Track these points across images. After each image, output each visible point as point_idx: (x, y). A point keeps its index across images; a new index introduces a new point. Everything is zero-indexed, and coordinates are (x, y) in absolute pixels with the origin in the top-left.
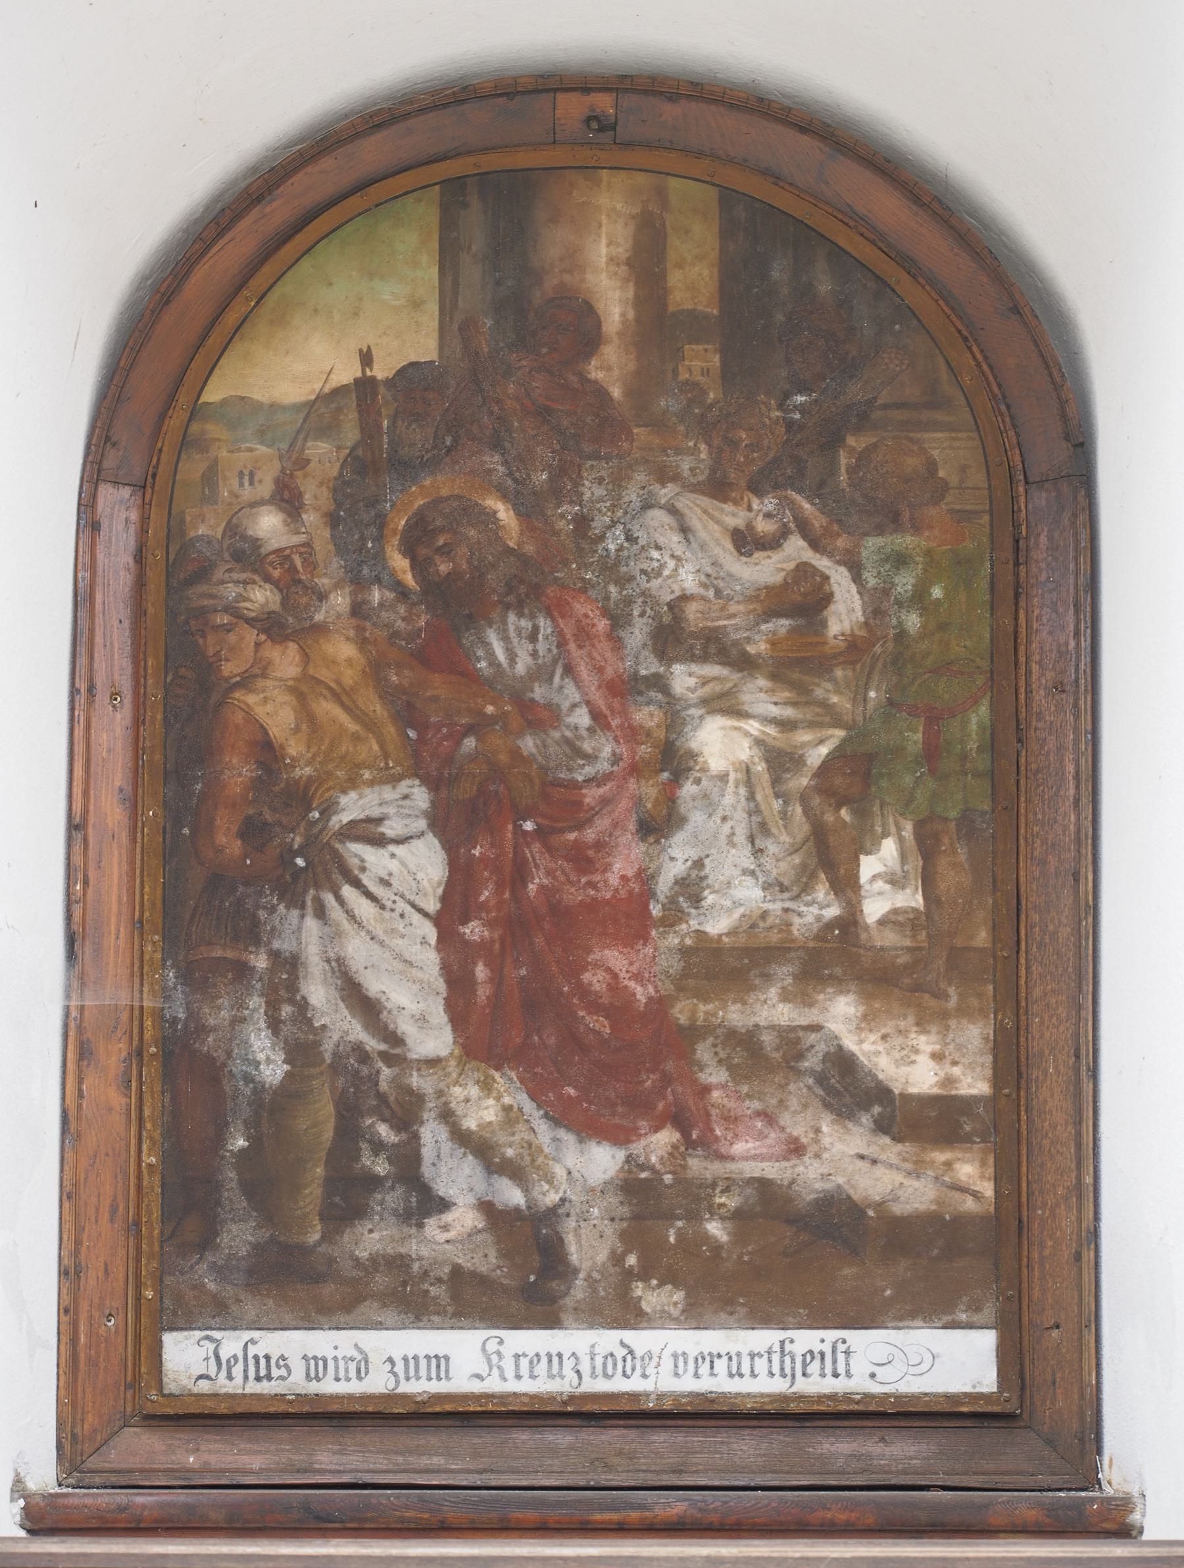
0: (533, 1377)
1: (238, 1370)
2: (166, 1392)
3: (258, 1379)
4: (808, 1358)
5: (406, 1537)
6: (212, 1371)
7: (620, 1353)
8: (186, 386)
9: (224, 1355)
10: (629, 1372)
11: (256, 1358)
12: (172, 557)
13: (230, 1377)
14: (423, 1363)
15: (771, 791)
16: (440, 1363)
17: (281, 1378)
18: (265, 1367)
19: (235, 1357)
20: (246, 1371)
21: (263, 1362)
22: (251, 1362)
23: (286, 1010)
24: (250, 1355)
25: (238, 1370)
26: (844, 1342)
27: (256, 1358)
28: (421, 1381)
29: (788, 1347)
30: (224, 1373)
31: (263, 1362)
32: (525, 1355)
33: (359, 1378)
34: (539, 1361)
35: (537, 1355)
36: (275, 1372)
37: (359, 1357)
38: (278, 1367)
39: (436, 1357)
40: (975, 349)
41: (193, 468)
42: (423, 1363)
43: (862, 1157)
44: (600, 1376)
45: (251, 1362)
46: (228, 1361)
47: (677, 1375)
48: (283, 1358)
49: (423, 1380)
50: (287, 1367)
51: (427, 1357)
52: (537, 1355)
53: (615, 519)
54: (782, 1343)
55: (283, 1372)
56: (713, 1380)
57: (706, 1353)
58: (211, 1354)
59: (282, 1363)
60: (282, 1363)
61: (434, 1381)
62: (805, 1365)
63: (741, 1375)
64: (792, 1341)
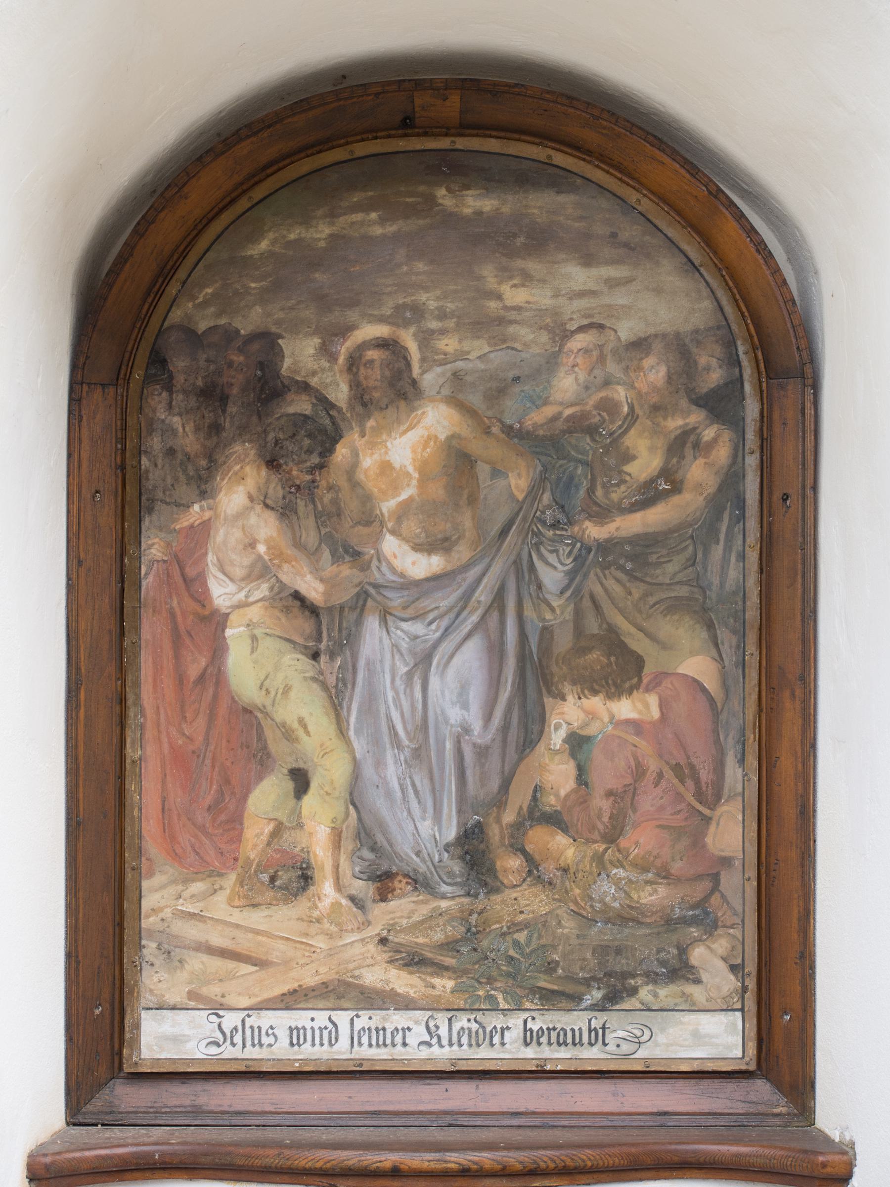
1: (238, 1039)
2: (752, 1067)
9: (227, 1027)
11: (252, 1027)
12: (487, 560)
14: (569, 1040)
17: (270, 1045)
21: (256, 1031)
22: (248, 1032)
24: (247, 1025)
25: (238, 1039)
28: (363, 1048)
30: (229, 1041)
32: (554, 1029)
33: (331, 1044)
34: (464, 1033)
36: (265, 1040)
37: (330, 1026)
38: (267, 1034)
42: (569, 1040)
43: (267, 677)
44: (555, 1044)
45: (248, 1032)
48: (272, 1028)
49: (455, 1047)
53: (576, 369)
54: (525, 1022)
55: (271, 1040)
59: (270, 1032)
60: (270, 1032)
63: (385, 1045)
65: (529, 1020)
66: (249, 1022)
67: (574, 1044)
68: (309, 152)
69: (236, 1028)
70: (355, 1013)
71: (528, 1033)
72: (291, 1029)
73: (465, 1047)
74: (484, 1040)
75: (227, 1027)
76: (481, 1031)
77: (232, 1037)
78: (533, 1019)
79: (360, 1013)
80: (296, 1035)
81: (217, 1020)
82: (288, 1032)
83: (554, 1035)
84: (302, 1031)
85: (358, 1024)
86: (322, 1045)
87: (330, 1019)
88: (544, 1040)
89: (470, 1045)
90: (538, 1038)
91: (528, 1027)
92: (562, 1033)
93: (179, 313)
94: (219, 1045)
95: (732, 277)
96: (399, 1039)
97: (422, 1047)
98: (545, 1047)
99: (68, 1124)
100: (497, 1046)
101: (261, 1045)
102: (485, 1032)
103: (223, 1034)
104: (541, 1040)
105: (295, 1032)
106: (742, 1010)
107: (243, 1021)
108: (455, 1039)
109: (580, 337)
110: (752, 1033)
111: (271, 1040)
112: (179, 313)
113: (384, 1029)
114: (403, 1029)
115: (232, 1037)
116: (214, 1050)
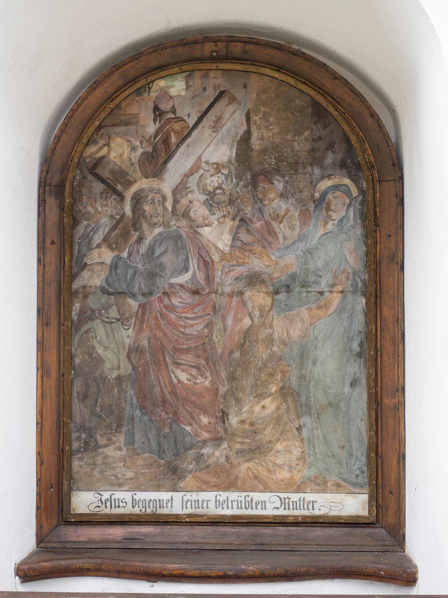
1: (108, 504)
2: (373, 519)
3: (293, 509)
5: (274, 581)
6: (100, 505)
8: (325, 83)
10: (247, 507)
11: (115, 499)
13: (106, 507)
16: (263, 504)
18: (250, 504)
19: (107, 499)
20: (191, 505)
21: (117, 501)
25: (108, 504)
26: (248, 496)
27: (115, 499)
29: (218, 498)
30: (104, 505)
31: (117, 501)
32: (234, 501)
34: (310, 503)
36: (121, 504)
41: (80, 230)
46: (138, 501)
47: (216, 508)
52: (224, 500)
54: (216, 496)
59: (123, 501)
62: (149, 503)
63: (297, 509)
64: (220, 496)
65: (218, 496)
66: (113, 497)
69: (168, 500)
71: (218, 502)
74: (219, 506)
77: (222, 505)
78: (220, 496)
80: (184, 504)
81: (100, 497)
85: (185, 499)
86: (232, 508)
90: (222, 505)
91: (218, 499)
92: (144, 501)
93: (78, 178)
95: (272, 65)
96: (205, 505)
97: (275, 510)
98: (299, 510)
99: (37, 548)
101: (119, 507)
103: (102, 503)
107: (216, 496)
112: (78, 178)
113: (198, 501)
114: (207, 500)
115: (106, 503)
116: (97, 509)
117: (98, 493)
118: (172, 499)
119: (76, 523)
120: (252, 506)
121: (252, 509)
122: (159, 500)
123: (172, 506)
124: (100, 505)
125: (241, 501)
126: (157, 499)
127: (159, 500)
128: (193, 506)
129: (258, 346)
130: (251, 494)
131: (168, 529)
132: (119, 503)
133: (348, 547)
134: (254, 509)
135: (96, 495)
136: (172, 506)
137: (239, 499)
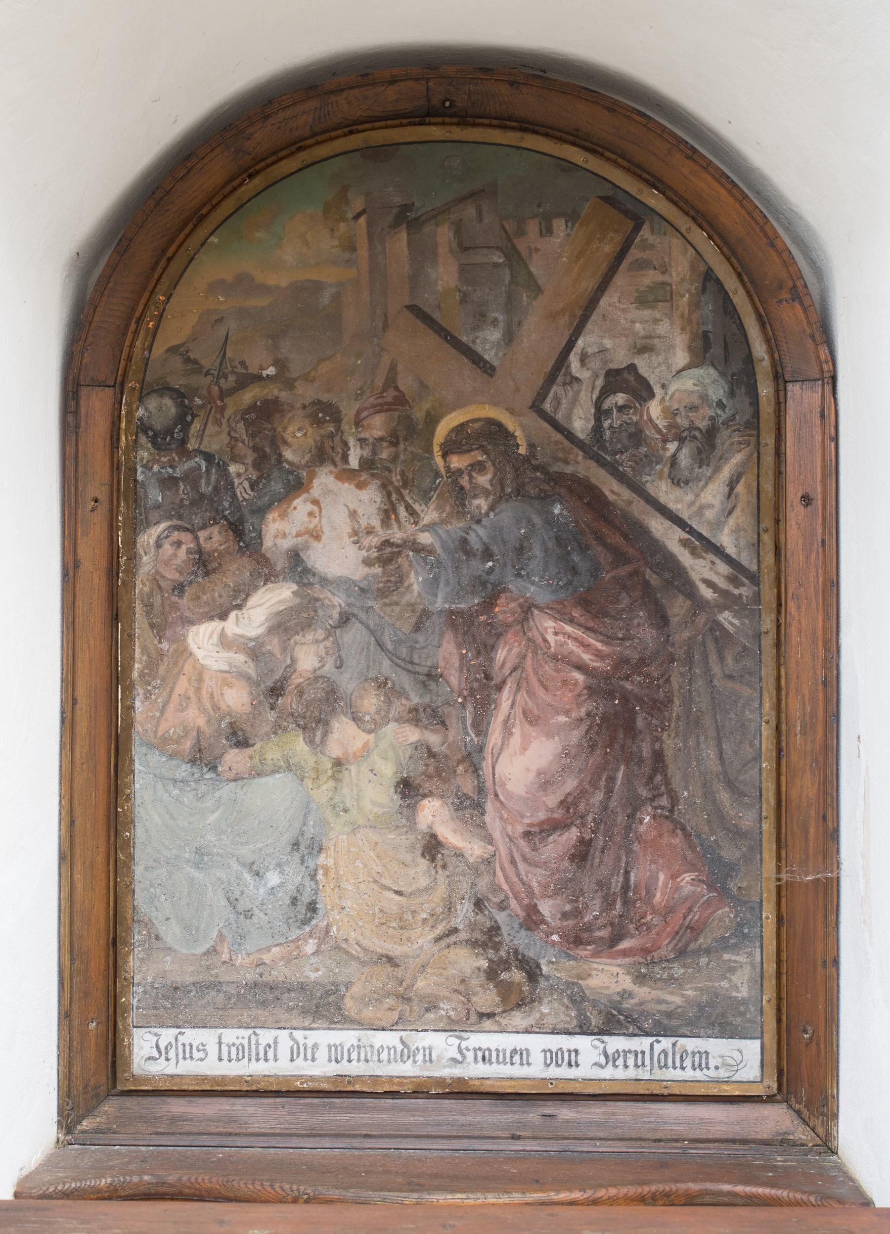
0: (683, 1068)
1: (172, 1054)
4: (616, 1055)
7: (400, 1047)
11: (184, 1045)
14: (494, 1059)
15: (146, 621)
17: (202, 1060)
23: (659, 778)
25: (172, 1054)
27: (184, 1045)
32: (234, 1045)
34: (619, 1056)
35: (382, 1046)
36: (196, 1055)
38: (199, 1051)
39: (699, 1052)
40: (258, 167)
46: (166, 1048)
50: (204, 1050)
51: (569, 1051)
52: (382, 1046)
56: (558, 1070)
57: (620, 1050)
58: (154, 1045)
59: (201, 1047)
60: (201, 1047)
61: (517, 1066)
62: (512, 1057)
67: (498, 1062)
68: (725, 249)
70: (654, 1038)
72: (330, 1046)
73: (354, 1063)
75: (610, 1051)
76: (406, 1051)
79: (660, 1039)
82: (327, 1049)
83: (480, 1054)
84: (339, 1048)
87: (401, 1039)
88: (620, 1062)
89: (522, 1064)
92: (240, 1047)
94: (602, 1067)
98: (495, 1065)
100: (621, 1067)
101: (191, 1057)
102: (409, 1052)
103: (160, 1053)
104: (617, 1063)
105: (333, 1048)
106: (762, 1038)
107: (176, 1039)
108: (262, 1055)
109: (169, 577)
110: (772, 1057)
111: (201, 1055)
117: (599, 1040)
118: (276, 1043)
119: (112, 816)
120: (305, 1055)
121: (350, 1061)
122: (497, 1050)
123: (275, 1056)
124: (156, 1055)
125: (243, 1047)
126: (427, 1046)
127: (497, 1050)
128: (225, 1056)
129: (636, 1005)
130: (682, 1041)
131: (155, 281)
132: (191, 1052)
133: (828, 507)
134: (271, 1061)
135: (597, 1043)
136: (275, 1056)
137: (237, 1042)
